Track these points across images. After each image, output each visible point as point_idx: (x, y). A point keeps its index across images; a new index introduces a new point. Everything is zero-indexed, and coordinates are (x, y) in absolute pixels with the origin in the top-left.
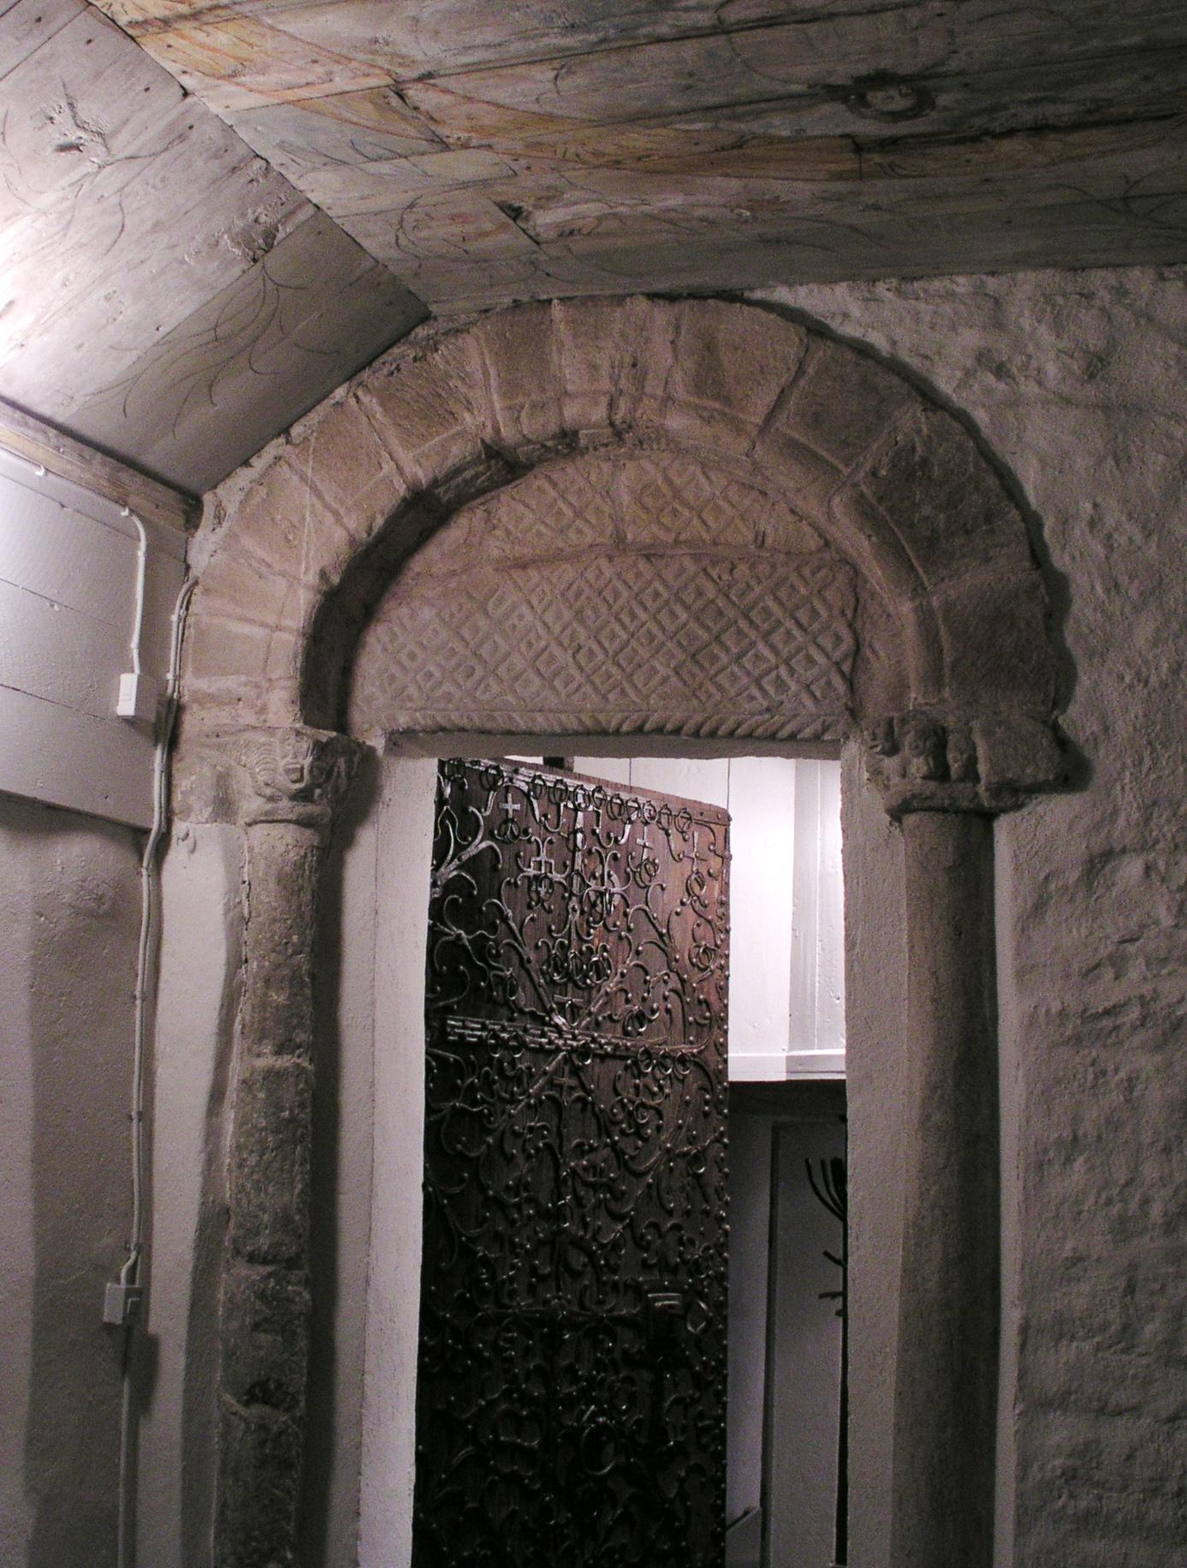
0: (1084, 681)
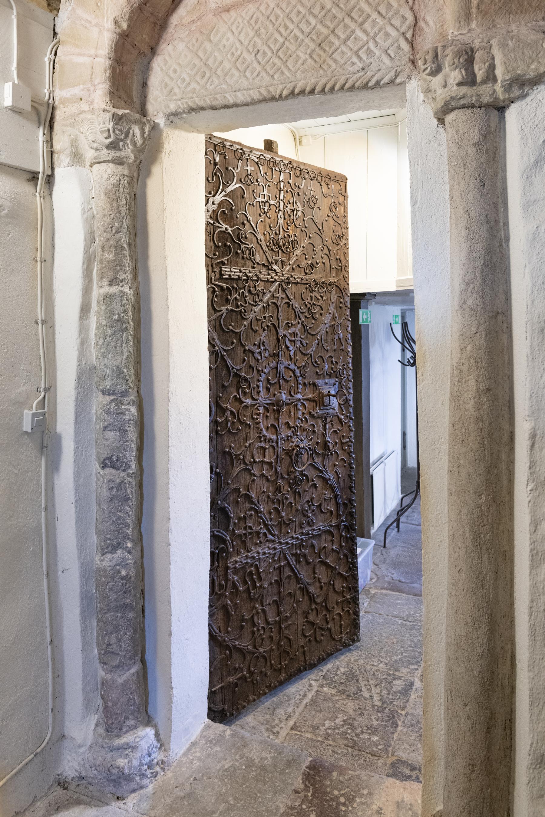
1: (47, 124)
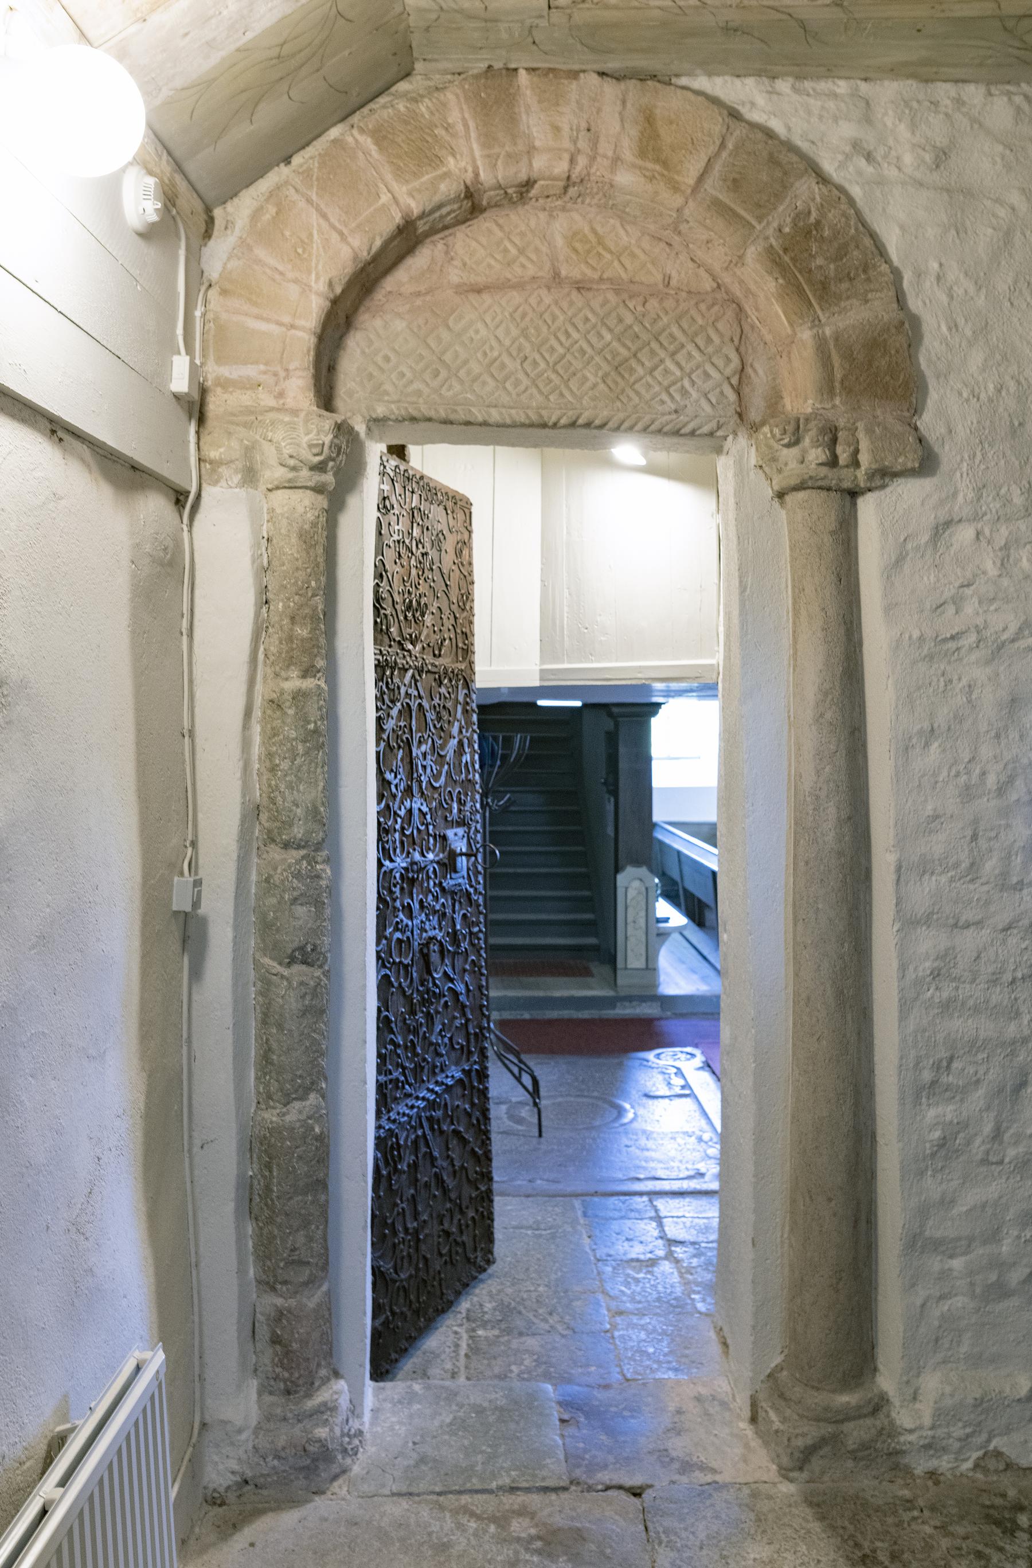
0: (933, 396)
1: (197, 415)
